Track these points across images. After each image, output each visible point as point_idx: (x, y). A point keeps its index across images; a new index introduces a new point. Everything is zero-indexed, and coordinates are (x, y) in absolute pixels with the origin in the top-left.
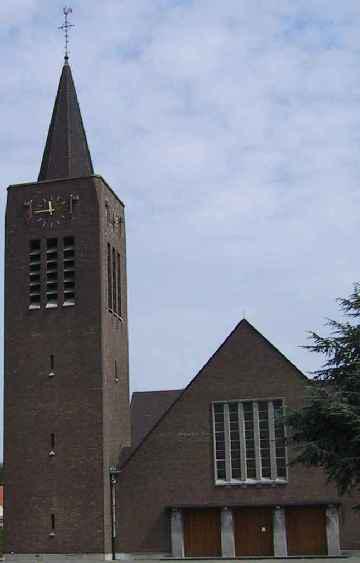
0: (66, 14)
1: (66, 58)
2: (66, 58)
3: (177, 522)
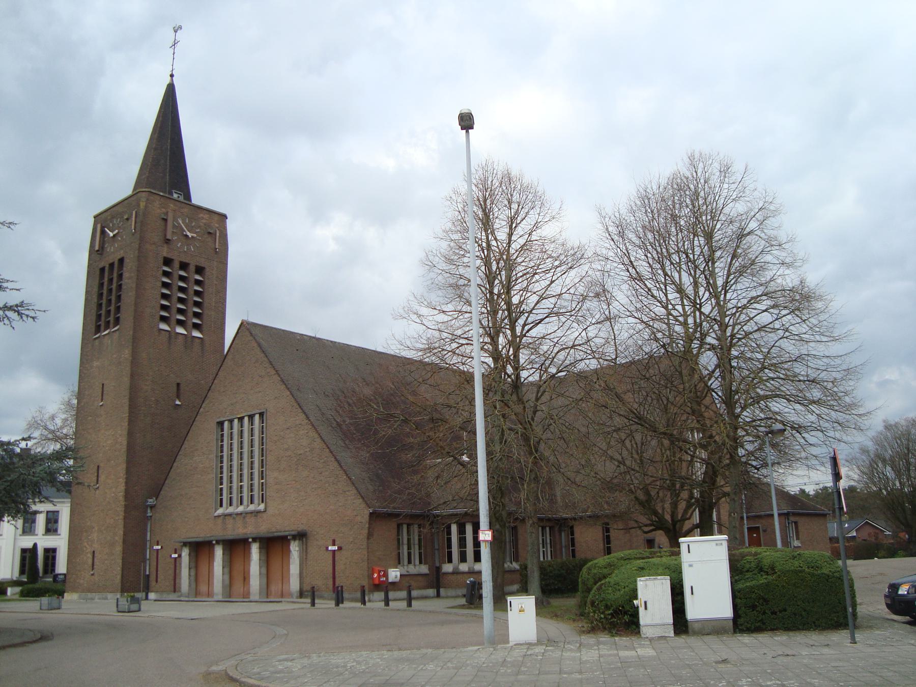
0: (176, 31)
1: (172, 76)
2: (172, 76)
3: (185, 553)
